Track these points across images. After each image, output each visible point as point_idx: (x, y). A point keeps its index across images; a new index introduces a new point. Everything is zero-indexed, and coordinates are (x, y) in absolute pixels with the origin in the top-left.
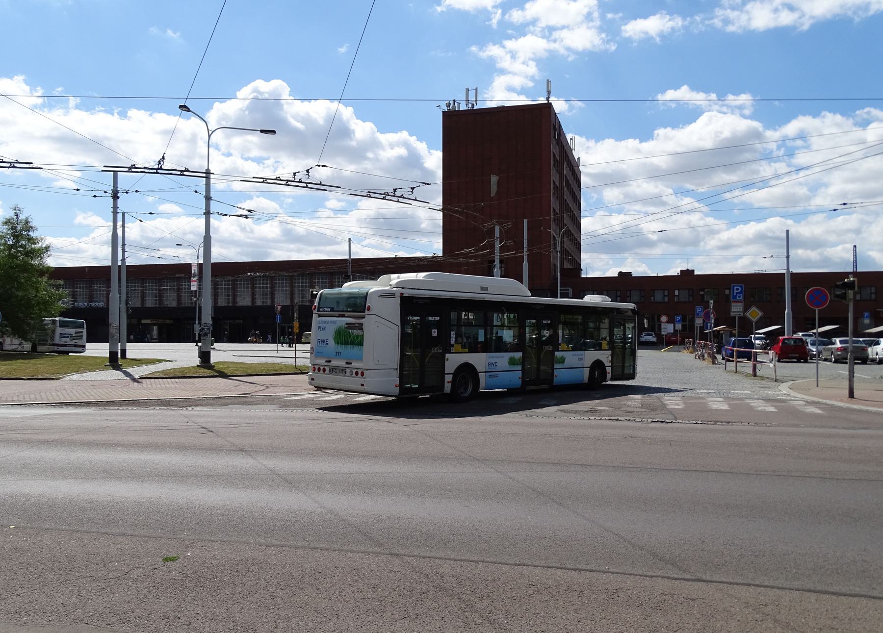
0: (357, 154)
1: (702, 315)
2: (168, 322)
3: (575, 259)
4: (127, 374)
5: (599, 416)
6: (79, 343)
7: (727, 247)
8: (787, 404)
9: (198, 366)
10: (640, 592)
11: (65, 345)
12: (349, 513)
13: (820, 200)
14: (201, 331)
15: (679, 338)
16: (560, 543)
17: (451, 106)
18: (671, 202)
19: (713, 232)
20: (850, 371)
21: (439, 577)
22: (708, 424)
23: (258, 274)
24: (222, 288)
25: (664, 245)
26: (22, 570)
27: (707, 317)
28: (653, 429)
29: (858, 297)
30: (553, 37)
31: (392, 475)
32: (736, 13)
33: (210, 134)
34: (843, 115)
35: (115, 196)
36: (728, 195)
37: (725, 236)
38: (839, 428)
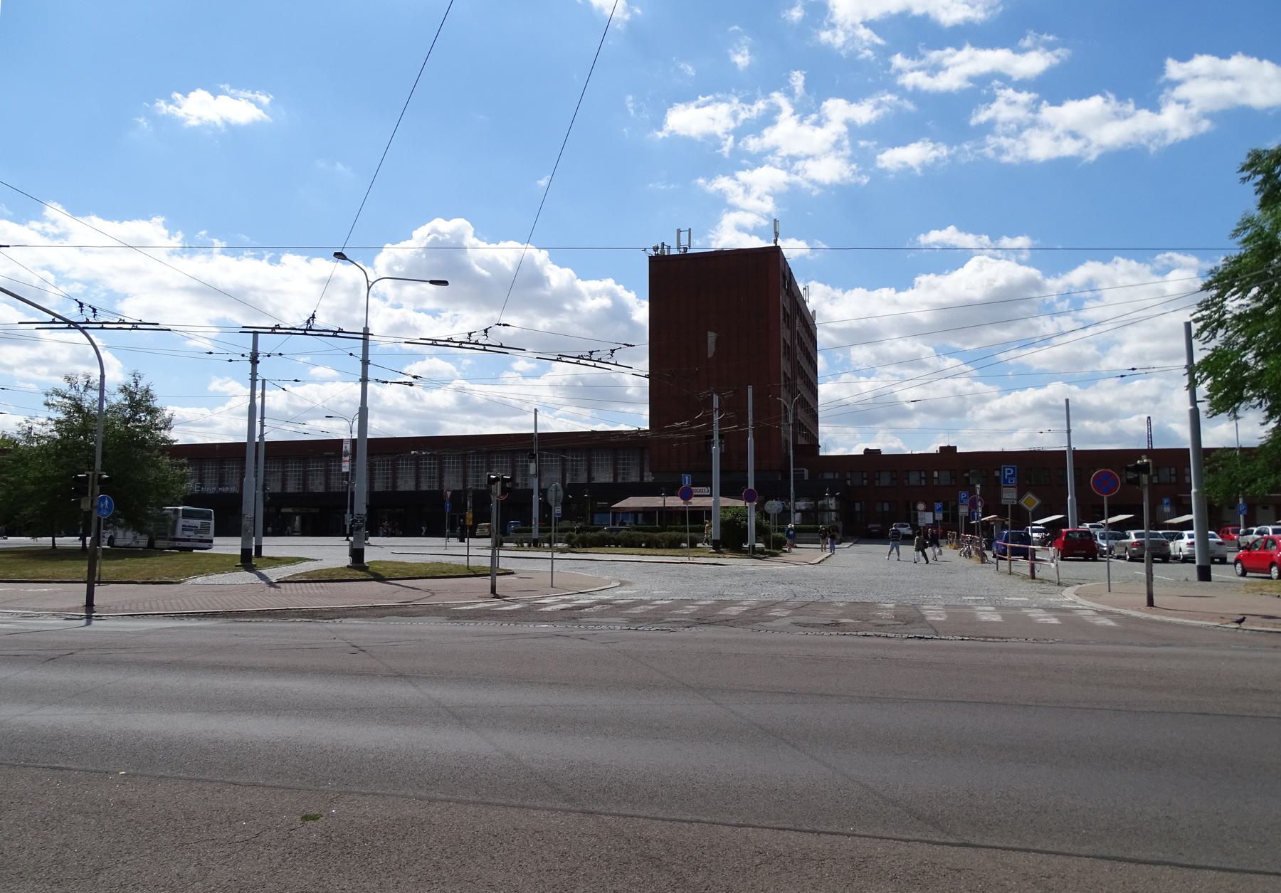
0: (552, 305)
1: (967, 502)
2: (313, 510)
3: (811, 433)
4: (262, 577)
5: (842, 631)
6: (206, 537)
7: (999, 418)
8: (1073, 615)
9: (348, 566)
10: (893, 861)
11: (188, 540)
12: (531, 757)
13: (1114, 362)
14: (353, 522)
15: (940, 531)
16: (794, 797)
17: (659, 250)
18: (931, 364)
19: (982, 400)
20: (1147, 573)
21: (644, 842)
22: (976, 640)
23: (424, 453)
24: (379, 469)
25: (922, 415)
26: (130, 830)
27: (973, 505)
28: (909, 647)
29: (1155, 480)
30: (795, 168)
31: (585, 708)
32: (1011, 141)
33: (370, 285)
34: (1139, 261)
35: (254, 360)
36: (1002, 356)
37: (997, 404)
38: (1136, 645)
